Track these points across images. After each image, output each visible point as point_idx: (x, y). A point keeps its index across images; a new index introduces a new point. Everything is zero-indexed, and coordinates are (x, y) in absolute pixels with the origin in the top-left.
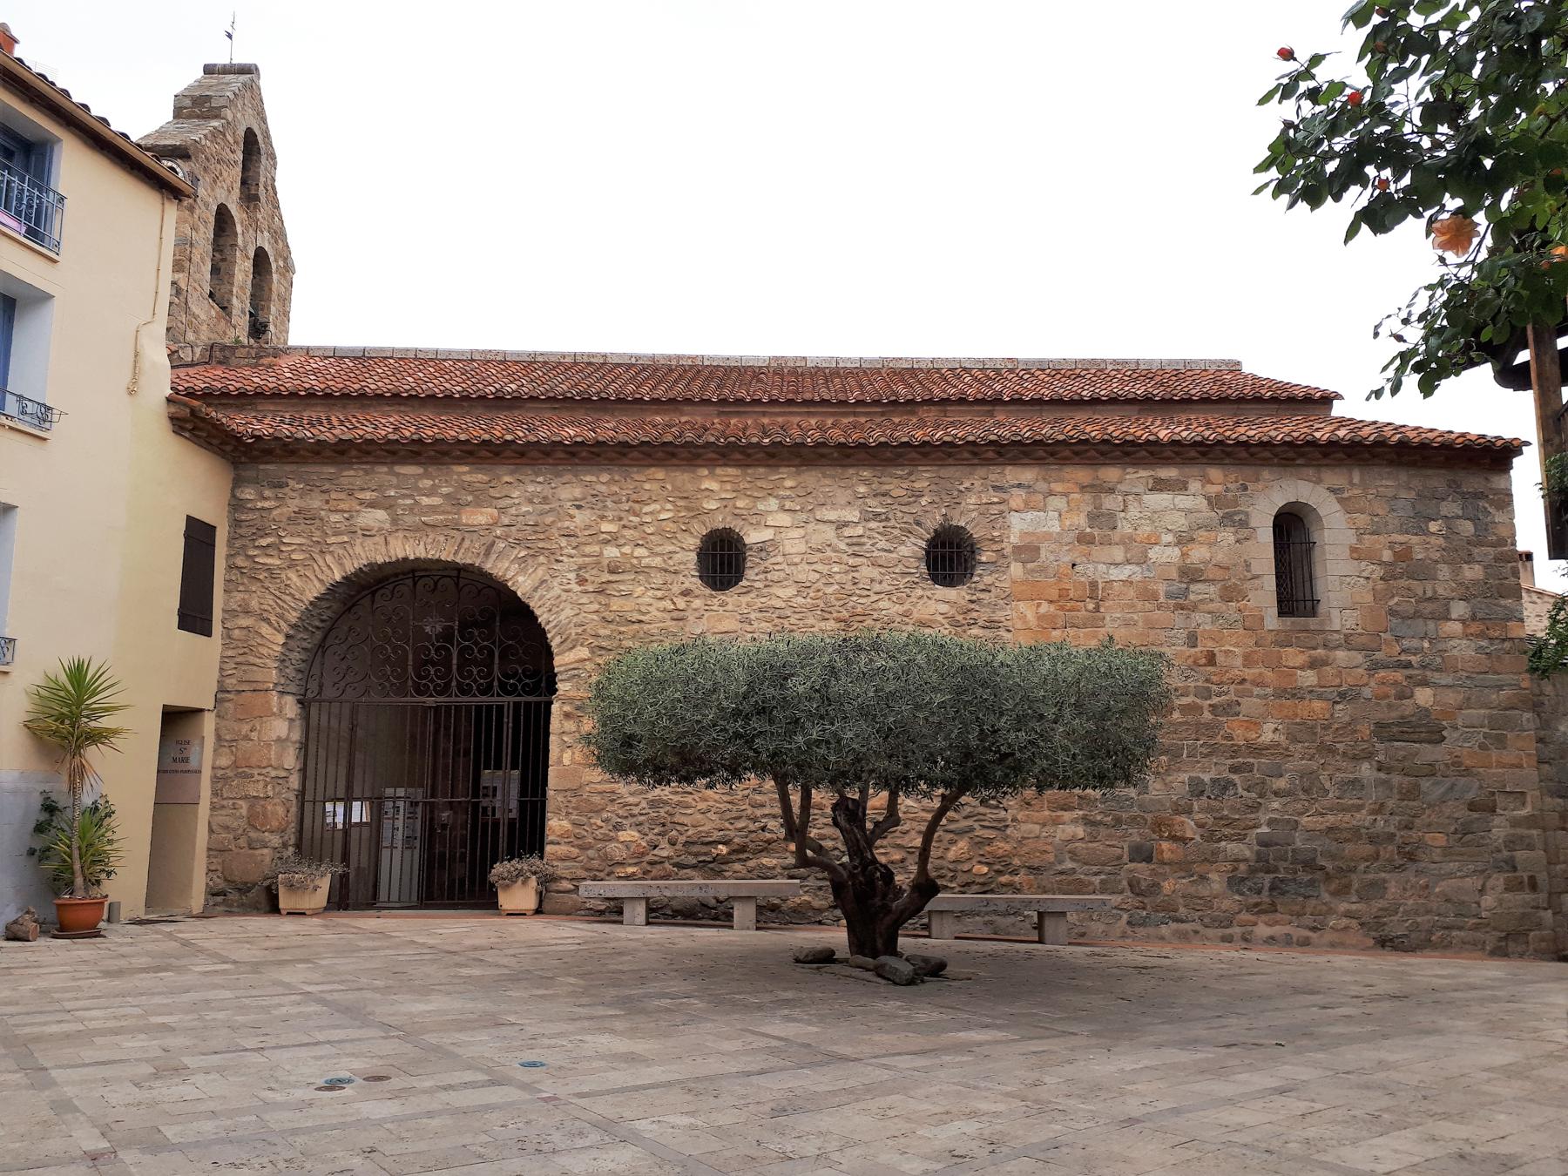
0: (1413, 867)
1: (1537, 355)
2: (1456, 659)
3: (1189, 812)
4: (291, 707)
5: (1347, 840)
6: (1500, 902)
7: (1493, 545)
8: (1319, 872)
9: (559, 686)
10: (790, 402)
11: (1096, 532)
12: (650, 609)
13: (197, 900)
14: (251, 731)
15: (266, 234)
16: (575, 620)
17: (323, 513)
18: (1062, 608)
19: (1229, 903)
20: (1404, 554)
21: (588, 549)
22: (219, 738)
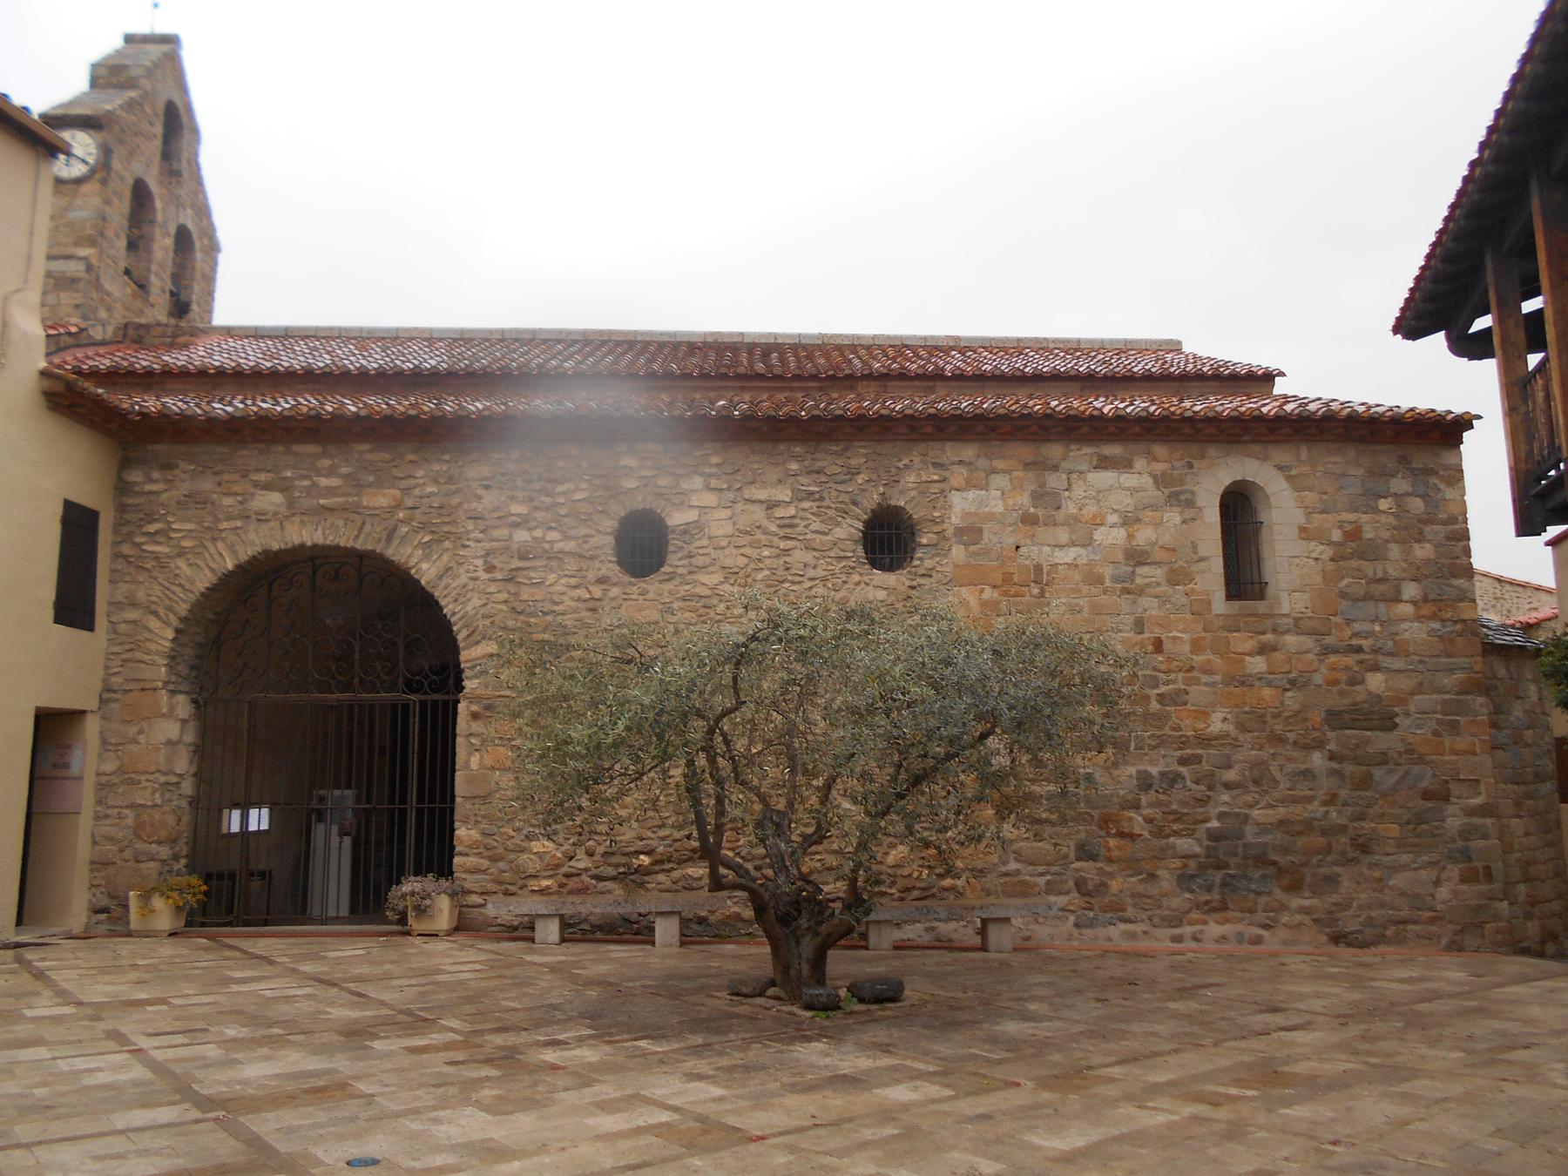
0: (1369, 859)
1: (1500, 320)
2: (1408, 643)
3: (1136, 806)
4: (183, 706)
5: (1301, 833)
6: (1456, 893)
7: (1445, 523)
8: (1272, 868)
9: (466, 683)
10: (724, 377)
11: (1041, 512)
12: (563, 598)
13: (78, 917)
14: (139, 733)
15: (189, 211)
16: (483, 611)
17: (214, 496)
18: (1005, 594)
19: (1179, 901)
20: (1353, 534)
21: (496, 533)
22: (104, 742)
